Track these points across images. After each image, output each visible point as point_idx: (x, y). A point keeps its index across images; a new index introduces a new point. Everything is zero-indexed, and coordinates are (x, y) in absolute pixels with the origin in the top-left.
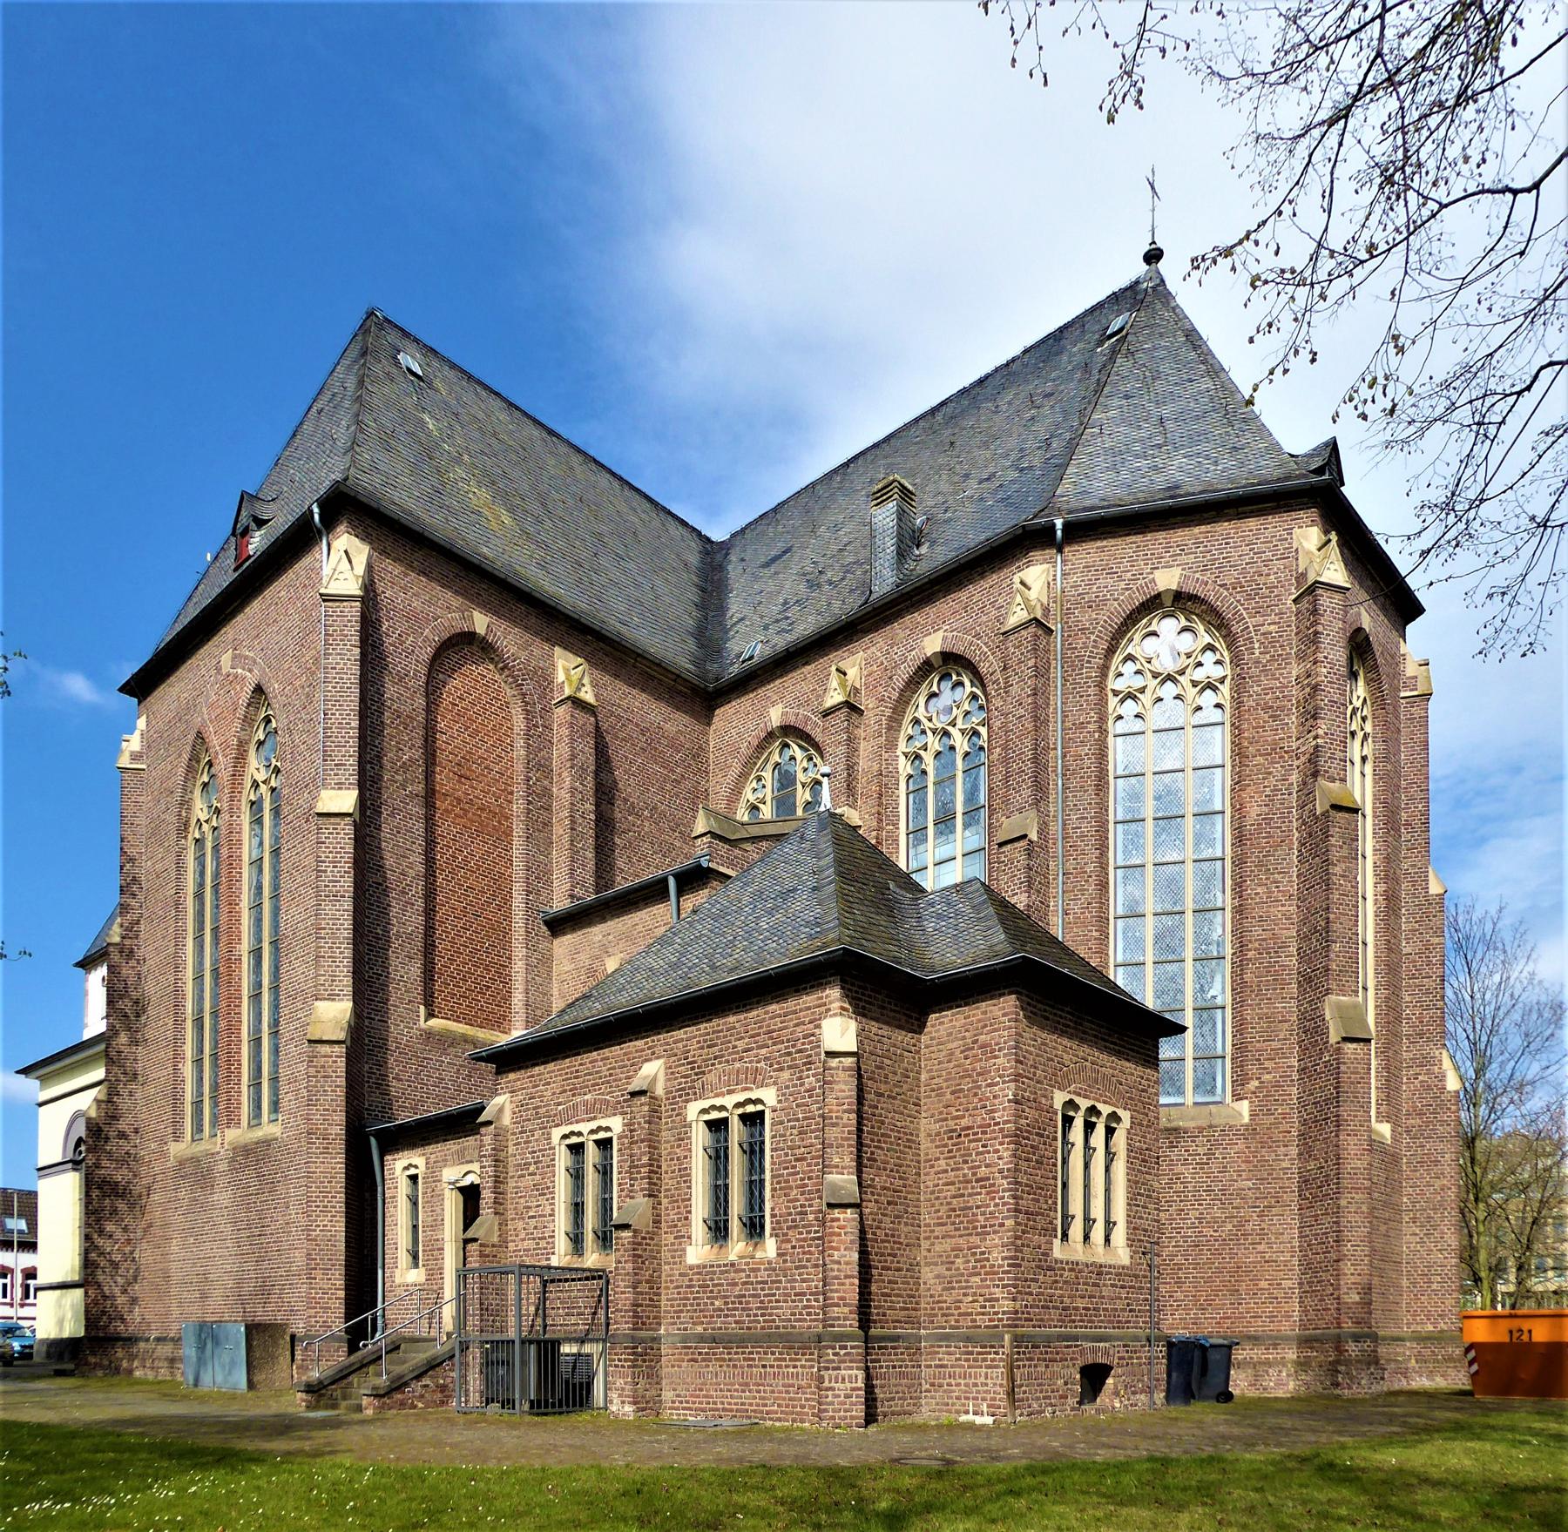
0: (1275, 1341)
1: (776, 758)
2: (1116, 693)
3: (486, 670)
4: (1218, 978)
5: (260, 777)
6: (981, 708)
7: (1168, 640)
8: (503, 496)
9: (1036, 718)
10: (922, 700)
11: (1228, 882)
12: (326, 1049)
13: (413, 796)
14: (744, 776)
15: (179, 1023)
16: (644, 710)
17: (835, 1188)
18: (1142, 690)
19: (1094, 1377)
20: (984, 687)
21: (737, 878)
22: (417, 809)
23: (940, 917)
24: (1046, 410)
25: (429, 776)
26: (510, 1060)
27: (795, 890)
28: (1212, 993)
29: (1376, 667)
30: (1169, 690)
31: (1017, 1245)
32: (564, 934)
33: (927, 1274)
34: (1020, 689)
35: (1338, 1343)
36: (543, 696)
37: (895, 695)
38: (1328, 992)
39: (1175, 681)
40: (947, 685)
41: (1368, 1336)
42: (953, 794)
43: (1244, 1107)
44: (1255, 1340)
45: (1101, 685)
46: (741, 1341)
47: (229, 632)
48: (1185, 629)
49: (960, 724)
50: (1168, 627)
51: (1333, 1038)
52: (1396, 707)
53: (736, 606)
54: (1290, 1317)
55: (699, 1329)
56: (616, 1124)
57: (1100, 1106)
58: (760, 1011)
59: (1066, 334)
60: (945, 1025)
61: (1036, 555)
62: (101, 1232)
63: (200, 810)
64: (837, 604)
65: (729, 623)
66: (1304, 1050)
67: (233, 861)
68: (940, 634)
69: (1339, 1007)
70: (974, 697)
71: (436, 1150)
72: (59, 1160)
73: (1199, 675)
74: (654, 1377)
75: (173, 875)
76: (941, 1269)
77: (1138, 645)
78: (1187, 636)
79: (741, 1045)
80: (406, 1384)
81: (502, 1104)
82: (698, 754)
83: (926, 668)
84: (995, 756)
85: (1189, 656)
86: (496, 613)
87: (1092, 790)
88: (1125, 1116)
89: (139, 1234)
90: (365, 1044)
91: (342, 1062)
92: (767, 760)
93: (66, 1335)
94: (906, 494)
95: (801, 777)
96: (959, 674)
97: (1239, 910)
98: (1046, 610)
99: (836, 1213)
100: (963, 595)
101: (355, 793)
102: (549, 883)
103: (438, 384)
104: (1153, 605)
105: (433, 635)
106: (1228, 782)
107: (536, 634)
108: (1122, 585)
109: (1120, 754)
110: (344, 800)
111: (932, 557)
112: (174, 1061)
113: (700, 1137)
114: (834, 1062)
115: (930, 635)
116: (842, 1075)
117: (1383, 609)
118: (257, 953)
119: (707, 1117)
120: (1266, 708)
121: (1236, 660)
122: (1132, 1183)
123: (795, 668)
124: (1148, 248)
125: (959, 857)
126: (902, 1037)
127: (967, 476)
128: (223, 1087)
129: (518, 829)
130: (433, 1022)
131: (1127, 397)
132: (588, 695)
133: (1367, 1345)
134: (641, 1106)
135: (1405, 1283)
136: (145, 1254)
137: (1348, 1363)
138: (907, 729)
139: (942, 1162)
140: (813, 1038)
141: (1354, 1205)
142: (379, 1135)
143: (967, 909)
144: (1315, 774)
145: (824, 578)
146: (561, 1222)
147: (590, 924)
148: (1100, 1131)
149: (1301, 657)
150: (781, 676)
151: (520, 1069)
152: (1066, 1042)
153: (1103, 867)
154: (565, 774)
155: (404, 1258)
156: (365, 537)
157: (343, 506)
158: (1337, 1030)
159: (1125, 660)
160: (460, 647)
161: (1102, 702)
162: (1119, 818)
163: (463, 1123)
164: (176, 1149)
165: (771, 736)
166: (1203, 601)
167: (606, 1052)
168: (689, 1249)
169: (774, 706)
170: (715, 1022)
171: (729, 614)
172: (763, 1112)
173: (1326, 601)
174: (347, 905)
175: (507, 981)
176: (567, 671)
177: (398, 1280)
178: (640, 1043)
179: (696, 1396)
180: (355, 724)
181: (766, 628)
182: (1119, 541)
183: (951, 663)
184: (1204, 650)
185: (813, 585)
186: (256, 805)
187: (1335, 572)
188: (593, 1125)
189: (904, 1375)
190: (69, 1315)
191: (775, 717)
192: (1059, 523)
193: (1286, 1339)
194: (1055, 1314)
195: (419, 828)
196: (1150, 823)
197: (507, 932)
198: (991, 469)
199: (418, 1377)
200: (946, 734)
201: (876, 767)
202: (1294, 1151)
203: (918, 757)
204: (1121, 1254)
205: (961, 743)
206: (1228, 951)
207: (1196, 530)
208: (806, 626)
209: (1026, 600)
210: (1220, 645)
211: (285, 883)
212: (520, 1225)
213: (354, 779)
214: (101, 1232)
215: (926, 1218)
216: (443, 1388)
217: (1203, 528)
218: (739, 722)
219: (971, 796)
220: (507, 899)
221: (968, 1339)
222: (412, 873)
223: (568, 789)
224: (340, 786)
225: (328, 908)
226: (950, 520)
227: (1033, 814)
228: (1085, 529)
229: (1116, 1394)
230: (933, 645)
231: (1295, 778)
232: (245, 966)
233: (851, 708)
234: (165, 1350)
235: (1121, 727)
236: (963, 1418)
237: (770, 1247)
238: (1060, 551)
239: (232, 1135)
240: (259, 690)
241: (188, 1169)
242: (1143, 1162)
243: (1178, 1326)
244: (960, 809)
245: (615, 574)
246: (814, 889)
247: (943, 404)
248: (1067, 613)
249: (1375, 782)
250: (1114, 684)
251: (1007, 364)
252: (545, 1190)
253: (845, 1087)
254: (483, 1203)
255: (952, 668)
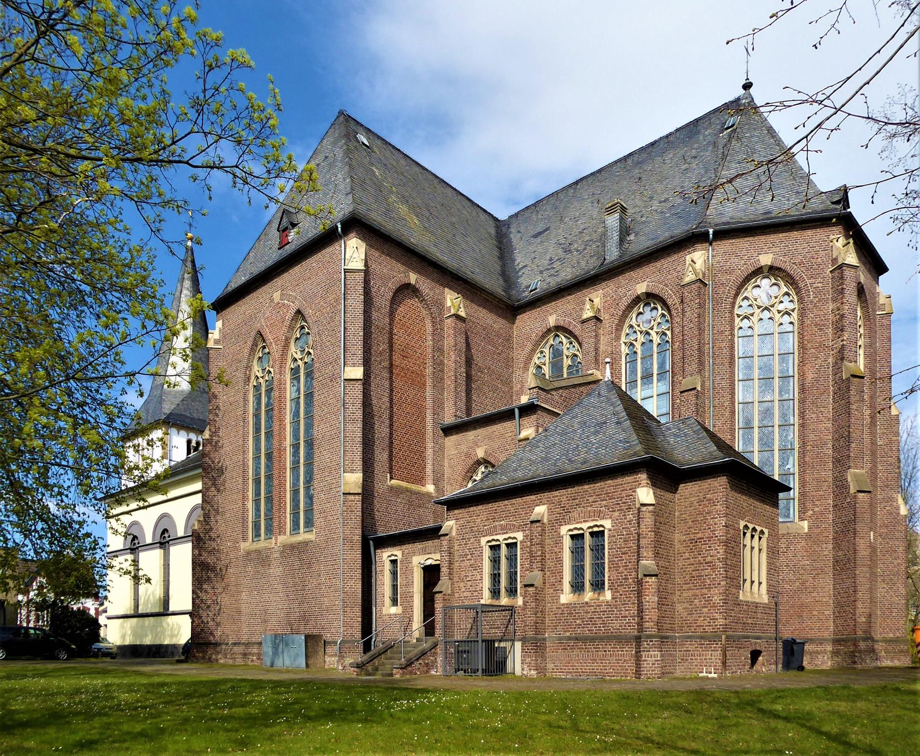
0: (821, 641)
1: (551, 342)
2: (739, 316)
3: (413, 302)
4: (791, 459)
5: (298, 356)
6: (667, 321)
7: (764, 290)
8: (413, 208)
9: (700, 329)
10: (634, 316)
11: (796, 411)
12: (352, 497)
13: (384, 368)
14: (533, 351)
15: (245, 481)
16: (486, 318)
17: (645, 566)
18: (752, 315)
19: (755, 655)
20: (669, 311)
21: (565, 414)
22: (386, 374)
23: (676, 436)
24: (694, 166)
25: (391, 356)
26: (454, 504)
27: (605, 423)
28: (788, 467)
29: (866, 301)
30: (766, 315)
31: (726, 593)
32: (452, 435)
33: (679, 607)
34: (691, 314)
35: (855, 642)
36: (440, 314)
37: (620, 313)
38: (849, 468)
39: (769, 310)
40: (648, 309)
41: (869, 638)
42: (652, 364)
43: (805, 524)
44: (811, 641)
45: (732, 312)
46: (593, 640)
47: (279, 281)
48: (774, 284)
49: (655, 329)
50: (765, 283)
51: (852, 490)
52: (875, 320)
53: (520, 259)
54: (828, 629)
55: (568, 634)
56: (519, 536)
57: (757, 527)
58: (602, 483)
59: (700, 123)
60: (688, 490)
61: (698, 246)
62: (201, 589)
63: (256, 369)
64: (583, 264)
65: (518, 268)
66: (836, 496)
67: (281, 399)
68: (646, 283)
69: (855, 475)
70: (663, 315)
71: (408, 547)
72: (122, 548)
73: (781, 307)
74: (544, 658)
75: (242, 404)
76: (687, 605)
77: (750, 291)
78: (775, 287)
79: (591, 499)
80: (413, 663)
81: (450, 525)
82: (509, 339)
83: (637, 300)
84: (676, 347)
85: (776, 298)
86: (419, 273)
87: (727, 365)
88: (766, 531)
89: (220, 590)
90: (367, 493)
91: (359, 504)
92: (547, 342)
93: (127, 643)
94: (623, 209)
95: (566, 352)
96: (654, 304)
97: (802, 426)
98: (704, 274)
99: (648, 579)
100: (658, 264)
101: (362, 369)
102: (443, 409)
103: (375, 149)
104: (758, 272)
105: (393, 286)
106: (796, 362)
107: (437, 282)
108: (743, 262)
109: (741, 347)
110: (357, 372)
111: (639, 243)
112: (240, 500)
113: (567, 543)
114: (644, 509)
115: (640, 283)
116: (649, 515)
117: (869, 271)
118: (296, 447)
119: (571, 533)
120: (816, 325)
121: (801, 300)
122: (769, 564)
123: (563, 297)
124: (744, 82)
125: (655, 397)
126: (669, 495)
127: (651, 198)
128: (276, 515)
129: (429, 382)
130: (393, 481)
131: (739, 163)
132: (462, 313)
133: (869, 643)
134: (537, 528)
135: (879, 613)
136: (225, 599)
137: (860, 652)
138: (626, 330)
139: (687, 554)
140: (632, 496)
141: (862, 573)
142: (374, 540)
143: (691, 433)
144: (842, 359)
145: (572, 247)
146: (486, 583)
147: (467, 431)
148: (756, 537)
149: (834, 300)
150: (555, 300)
151: (461, 508)
152: (744, 497)
153: (733, 403)
154: (452, 353)
155: (388, 601)
156: (363, 239)
157: (353, 224)
158: (854, 487)
159: (743, 300)
160: (406, 290)
161: (732, 321)
162: (741, 378)
163: (433, 533)
164: (245, 546)
165: (549, 331)
166: (784, 271)
167: (514, 501)
168: (562, 596)
169: (552, 316)
170: (576, 488)
171: (516, 263)
172: (603, 531)
173: (848, 273)
174: (360, 425)
175: (422, 458)
176: (451, 300)
177: (384, 613)
178: (533, 497)
179: (567, 668)
180: (361, 334)
181: (541, 272)
182: (741, 240)
183: (650, 298)
184: (784, 295)
185: (567, 251)
186: (295, 371)
187: (852, 258)
188: (506, 536)
189: (671, 655)
190: (129, 632)
191: (552, 321)
192: (711, 231)
193: (826, 640)
194: (740, 626)
195: (387, 383)
196: (756, 381)
197: (424, 434)
198: (666, 196)
199: (417, 660)
200: (648, 333)
201: (610, 349)
202: (830, 546)
203: (632, 344)
204: (765, 599)
205: (656, 339)
206: (797, 446)
207: (781, 235)
208: (567, 274)
209: (694, 270)
210: (792, 292)
211: (317, 412)
212: (462, 584)
213: (361, 361)
214: (201, 589)
215: (678, 580)
216: (427, 665)
217: (784, 234)
218: (528, 324)
219: (661, 365)
220: (424, 419)
221: (702, 638)
222: (384, 407)
223: (452, 361)
224: (354, 365)
225: (349, 426)
226: (645, 222)
227: (699, 377)
228: (725, 233)
229: (763, 665)
230: (641, 288)
231: (831, 360)
232: (288, 452)
233: (597, 319)
234: (239, 649)
235: (741, 333)
236: (701, 675)
237: (608, 595)
238: (711, 244)
239: (282, 539)
240: (299, 312)
241: (253, 556)
242: (773, 553)
243: (787, 634)
244: (655, 372)
245: (464, 246)
246: (617, 423)
247: (630, 155)
248: (715, 275)
249: (865, 358)
250: (737, 311)
251: (667, 136)
252: (478, 568)
253: (648, 520)
254: (442, 574)
255: (649, 300)
